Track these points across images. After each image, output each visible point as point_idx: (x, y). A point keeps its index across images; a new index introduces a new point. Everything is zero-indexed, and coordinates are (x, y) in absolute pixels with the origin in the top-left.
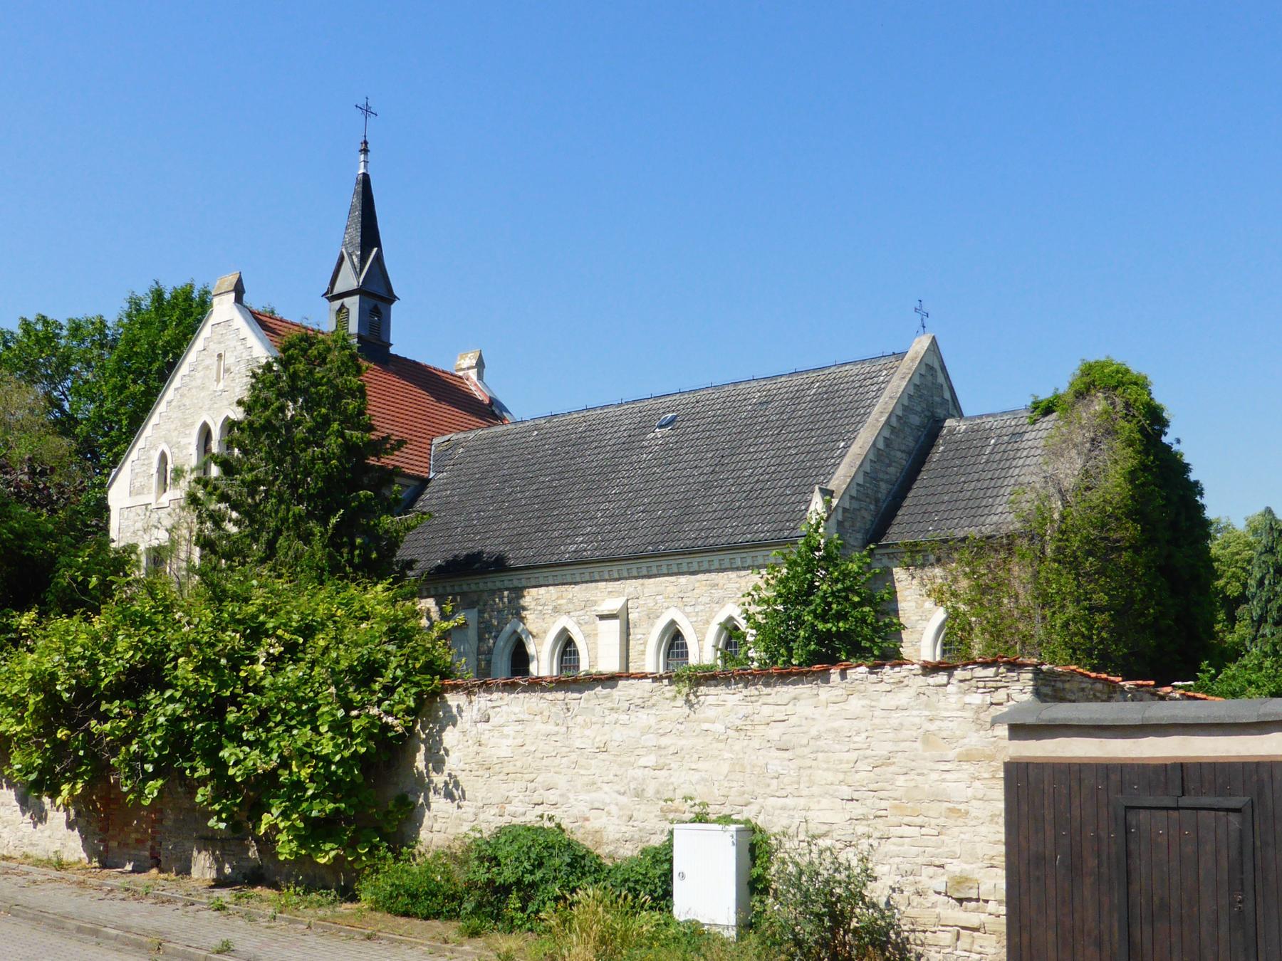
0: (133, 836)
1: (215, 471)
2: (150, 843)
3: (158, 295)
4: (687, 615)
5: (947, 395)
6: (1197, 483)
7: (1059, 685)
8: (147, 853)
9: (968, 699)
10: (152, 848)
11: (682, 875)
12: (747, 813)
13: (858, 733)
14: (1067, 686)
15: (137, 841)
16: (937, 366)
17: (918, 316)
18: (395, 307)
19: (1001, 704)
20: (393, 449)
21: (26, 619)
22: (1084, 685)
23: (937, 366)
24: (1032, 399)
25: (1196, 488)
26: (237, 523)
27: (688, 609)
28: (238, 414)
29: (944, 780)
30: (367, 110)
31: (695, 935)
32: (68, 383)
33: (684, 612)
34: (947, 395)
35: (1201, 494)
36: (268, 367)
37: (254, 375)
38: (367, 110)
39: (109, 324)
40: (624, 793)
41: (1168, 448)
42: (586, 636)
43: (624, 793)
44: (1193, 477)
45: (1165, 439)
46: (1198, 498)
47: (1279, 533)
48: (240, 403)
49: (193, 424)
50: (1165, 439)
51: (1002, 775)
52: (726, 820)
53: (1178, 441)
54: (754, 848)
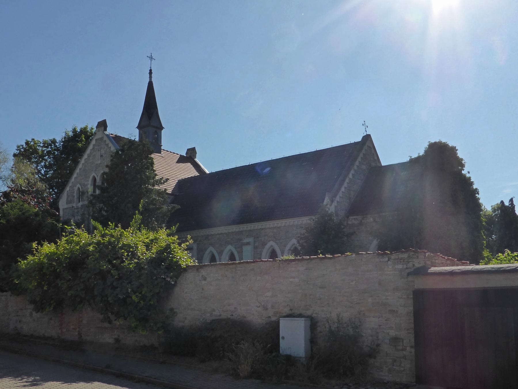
0: (72, 327)
1: (98, 192)
2: (78, 329)
3: (74, 131)
4: (277, 244)
5: (376, 158)
6: (476, 189)
7: (433, 261)
8: (77, 333)
9: (396, 267)
10: (79, 331)
11: (283, 338)
12: (309, 313)
13: (352, 281)
14: (437, 261)
15: (73, 329)
16: (372, 146)
17: (364, 127)
18: (163, 131)
19: (410, 268)
20: (164, 182)
21: (34, 245)
22: (443, 261)
23: (372, 146)
24: (409, 158)
25: (476, 191)
26: (106, 211)
27: (277, 241)
28: (107, 170)
29: (387, 299)
30: (151, 58)
31: (290, 360)
32: (43, 164)
33: (276, 243)
34: (376, 158)
35: (478, 194)
36: (117, 152)
37: (112, 156)
38: (151, 58)
39: (58, 141)
40: (259, 307)
41: (464, 176)
42: (238, 252)
43: (259, 307)
44: (475, 187)
45: (463, 172)
46: (477, 195)
47: (506, 211)
48: (107, 166)
49: (89, 177)
50: (463, 172)
51: (412, 296)
52: (300, 316)
53: (469, 172)
54: (313, 324)
